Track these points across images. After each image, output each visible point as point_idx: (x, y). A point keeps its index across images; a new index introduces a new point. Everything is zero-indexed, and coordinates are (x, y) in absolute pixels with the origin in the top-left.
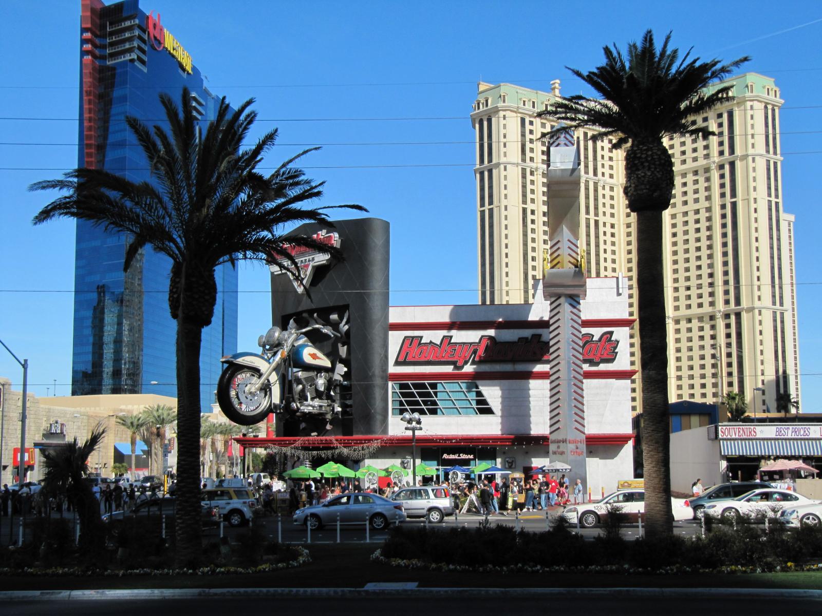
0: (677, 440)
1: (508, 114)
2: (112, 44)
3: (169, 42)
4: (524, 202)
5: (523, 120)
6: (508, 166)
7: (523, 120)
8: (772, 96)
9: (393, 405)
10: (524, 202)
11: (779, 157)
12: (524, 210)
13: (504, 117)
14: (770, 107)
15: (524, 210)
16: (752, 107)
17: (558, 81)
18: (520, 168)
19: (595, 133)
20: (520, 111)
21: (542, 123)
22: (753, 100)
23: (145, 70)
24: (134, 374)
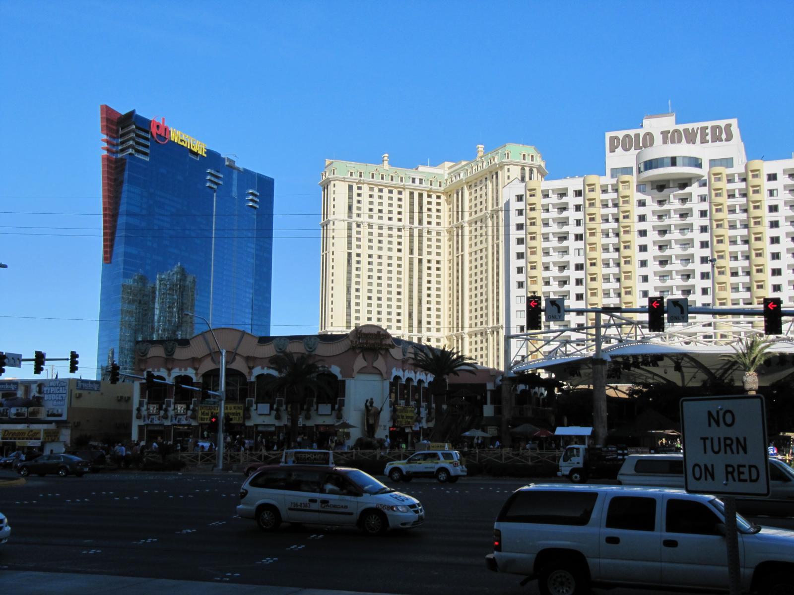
0: (594, 314)
1: (511, 167)
2: (122, 143)
3: (175, 136)
4: (349, 247)
5: (350, 188)
6: (336, 222)
7: (350, 188)
8: (528, 160)
9: (225, 409)
10: (349, 247)
11: (322, 254)
12: (349, 254)
13: (509, 170)
14: (527, 169)
15: (349, 254)
16: (509, 169)
17: (387, 155)
18: (346, 223)
19: (540, 177)
20: (346, 180)
21: (370, 187)
22: (334, 180)
23: (147, 159)
24: (140, 361)
